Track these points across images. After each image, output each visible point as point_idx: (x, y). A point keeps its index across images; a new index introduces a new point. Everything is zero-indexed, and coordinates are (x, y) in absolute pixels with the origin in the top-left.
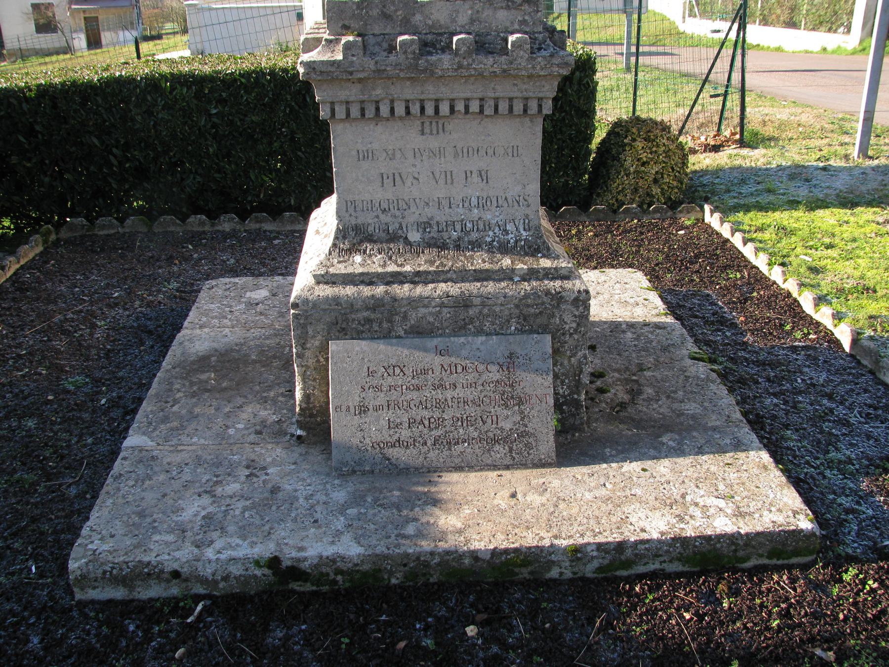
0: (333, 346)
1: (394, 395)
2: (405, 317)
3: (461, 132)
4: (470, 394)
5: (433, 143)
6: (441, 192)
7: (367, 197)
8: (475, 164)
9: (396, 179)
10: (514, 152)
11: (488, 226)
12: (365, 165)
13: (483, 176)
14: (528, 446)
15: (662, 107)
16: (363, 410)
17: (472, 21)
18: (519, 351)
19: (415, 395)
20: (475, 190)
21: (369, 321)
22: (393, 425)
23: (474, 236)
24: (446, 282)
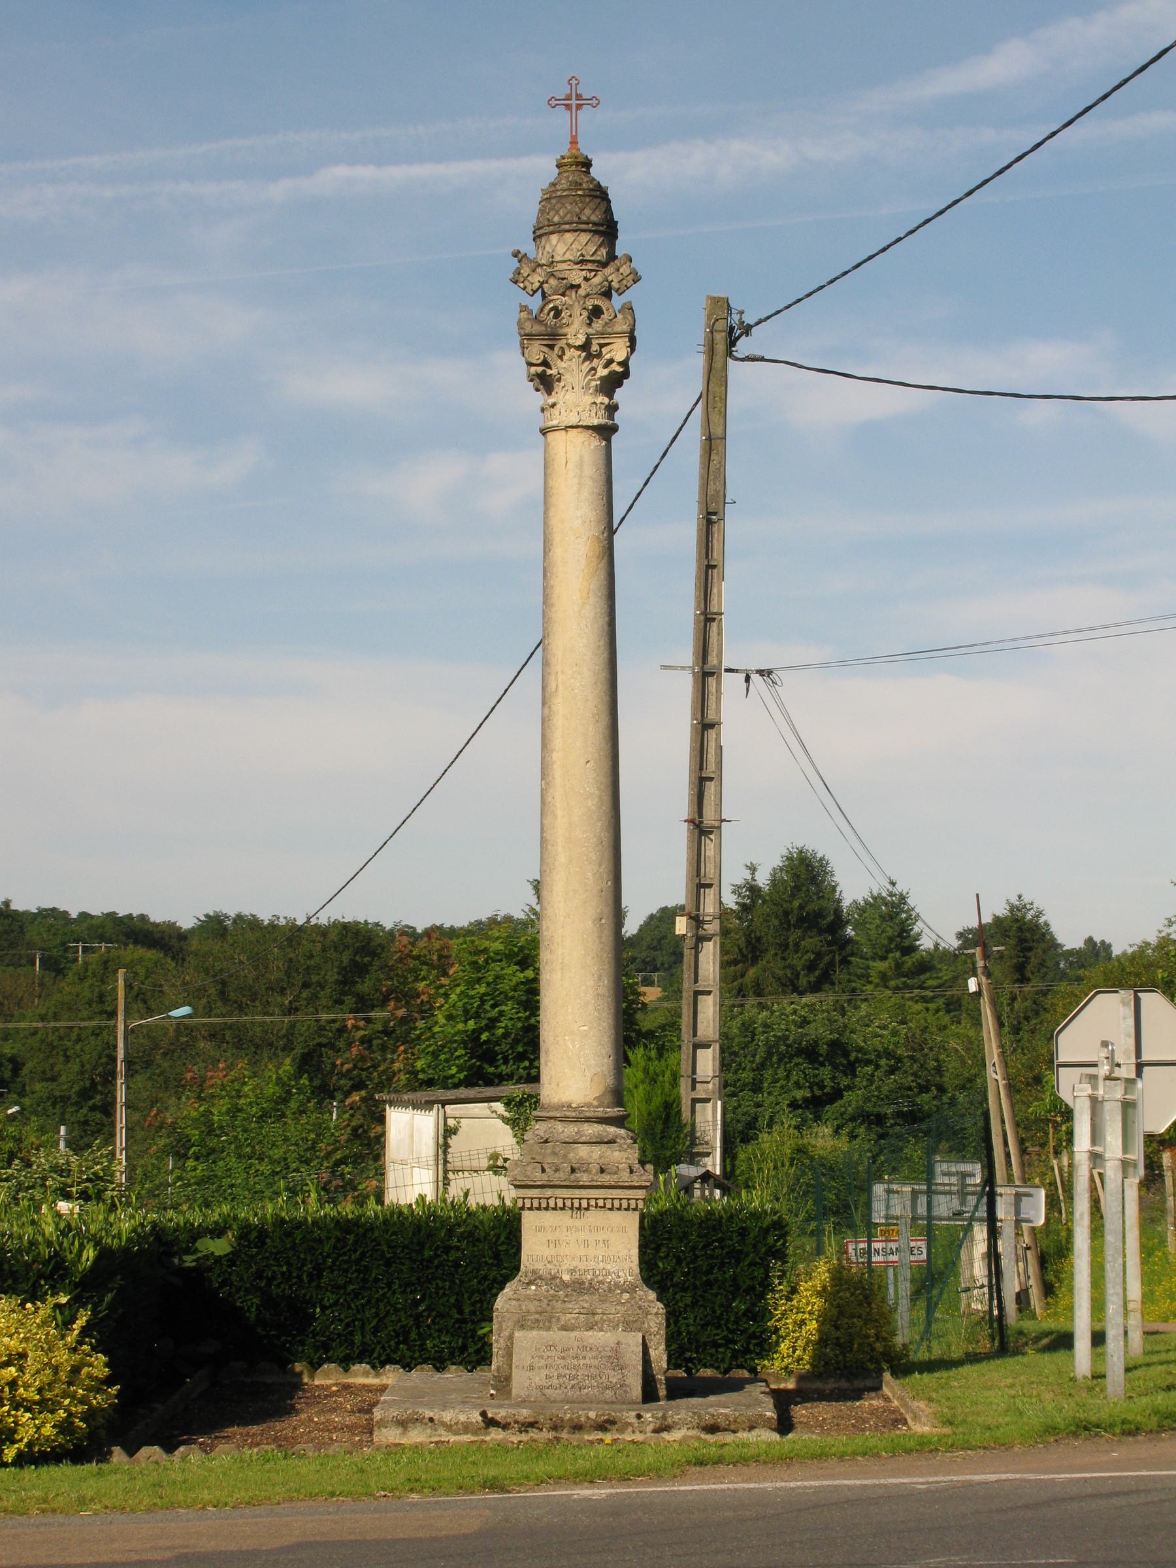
0: (517, 1334)
1: (550, 1361)
2: (559, 1319)
3: (594, 1217)
6: (582, 1252)
8: (601, 1236)
9: (556, 1243)
10: (624, 1230)
12: (540, 1235)
16: (532, 1368)
17: (601, 1157)
18: (623, 1341)
19: (561, 1361)
20: (601, 1251)
22: (548, 1377)
23: (601, 1278)
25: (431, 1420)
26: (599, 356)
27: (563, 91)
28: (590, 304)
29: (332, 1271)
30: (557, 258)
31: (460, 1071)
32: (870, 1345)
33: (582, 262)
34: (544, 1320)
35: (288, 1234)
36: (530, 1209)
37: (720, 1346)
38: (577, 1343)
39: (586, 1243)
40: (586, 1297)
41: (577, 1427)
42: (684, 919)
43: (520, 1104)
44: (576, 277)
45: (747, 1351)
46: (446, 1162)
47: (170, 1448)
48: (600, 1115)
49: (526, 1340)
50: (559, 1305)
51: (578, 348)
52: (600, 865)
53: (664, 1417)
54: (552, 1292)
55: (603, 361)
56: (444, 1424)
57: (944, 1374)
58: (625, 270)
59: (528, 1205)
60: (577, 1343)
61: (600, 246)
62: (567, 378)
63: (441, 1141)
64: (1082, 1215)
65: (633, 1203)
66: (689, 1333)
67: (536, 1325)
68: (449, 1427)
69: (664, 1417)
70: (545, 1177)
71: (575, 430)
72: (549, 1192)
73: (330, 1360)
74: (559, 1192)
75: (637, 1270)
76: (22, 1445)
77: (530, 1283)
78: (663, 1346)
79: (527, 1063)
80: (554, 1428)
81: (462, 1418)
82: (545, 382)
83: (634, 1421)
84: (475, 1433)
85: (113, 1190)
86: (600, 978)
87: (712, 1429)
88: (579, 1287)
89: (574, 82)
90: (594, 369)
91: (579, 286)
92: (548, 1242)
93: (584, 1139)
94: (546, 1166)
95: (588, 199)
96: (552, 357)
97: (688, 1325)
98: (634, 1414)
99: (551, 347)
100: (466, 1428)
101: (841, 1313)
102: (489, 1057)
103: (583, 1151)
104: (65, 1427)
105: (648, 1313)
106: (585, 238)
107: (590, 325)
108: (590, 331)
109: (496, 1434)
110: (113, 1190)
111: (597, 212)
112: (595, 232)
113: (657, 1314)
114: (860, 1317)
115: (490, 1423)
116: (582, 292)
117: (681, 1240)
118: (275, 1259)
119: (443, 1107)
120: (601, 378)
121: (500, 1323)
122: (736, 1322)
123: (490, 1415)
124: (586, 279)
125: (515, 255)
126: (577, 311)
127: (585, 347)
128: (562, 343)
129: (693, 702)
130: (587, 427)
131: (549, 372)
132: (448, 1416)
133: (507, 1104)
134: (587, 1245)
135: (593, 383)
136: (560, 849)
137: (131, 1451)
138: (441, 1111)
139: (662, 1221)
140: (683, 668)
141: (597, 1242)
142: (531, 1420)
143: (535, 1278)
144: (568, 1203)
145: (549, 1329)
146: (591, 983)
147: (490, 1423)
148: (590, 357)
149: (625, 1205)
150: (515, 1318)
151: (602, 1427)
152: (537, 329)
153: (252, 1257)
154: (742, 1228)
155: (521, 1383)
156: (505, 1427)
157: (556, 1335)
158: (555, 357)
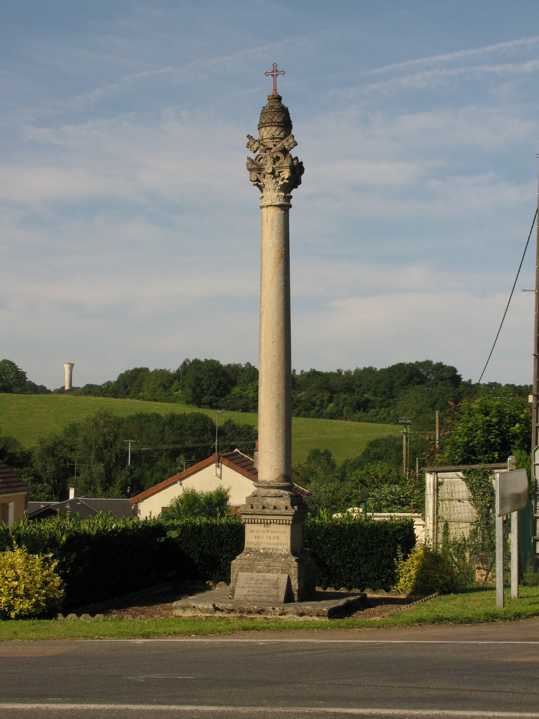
2: (256, 568)
3: (273, 527)
4: (268, 586)
5: (266, 529)
7: (252, 541)
8: (276, 535)
10: (285, 532)
11: (278, 550)
13: (278, 538)
14: (278, 598)
15: (51, 621)
16: (243, 587)
17: (276, 503)
18: (280, 577)
20: (276, 541)
21: (248, 568)
22: (249, 591)
24: (32, 550)
25: (194, 607)
26: (279, 176)
27: (279, 69)
28: (275, 156)
29: (226, 545)
30: (264, 137)
31: (459, 458)
32: (437, 581)
33: (273, 138)
34: (250, 568)
35: (210, 529)
36: (248, 523)
37: (377, 579)
38: (262, 578)
39: (270, 538)
40: (268, 559)
41: (250, 612)
42: (532, 396)
43: (469, 472)
44: (270, 145)
45: (387, 582)
46: (437, 496)
47: (93, 615)
48: (277, 485)
49: (243, 576)
50: (256, 562)
51: (270, 174)
52: (278, 384)
53: (283, 609)
54: (255, 557)
55: (281, 179)
56: (199, 609)
57: (484, 592)
58: (291, 141)
59: (247, 521)
60: (262, 578)
61: (281, 132)
62: (267, 186)
63: (435, 488)
64: (514, 529)
65: (288, 521)
66: (364, 574)
67: (247, 570)
68: (201, 610)
69: (283, 609)
70: (252, 510)
71: (271, 207)
72: (255, 517)
73: (222, 580)
74: (258, 517)
75: (289, 549)
76: (17, 612)
77: (247, 553)
78: (296, 580)
79: (488, 455)
80: (241, 612)
81: (206, 607)
82: (261, 188)
83: (272, 610)
84: (211, 613)
85: (414, 501)
86: (278, 430)
87: (301, 615)
88: (266, 555)
89: (275, 65)
90: (277, 182)
91: (271, 148)
92: (256, 536)
93: (269, 495)
94: (254, 506)
95: (276, 113)
96: (261, 177)
97: (364, 570)
98: (271, 607)
99: (260, 174)
100: (207, 611)
101: (425, 568)
102: (474, 453)
103: (269, 500)
104: (36, 605)
105: (291, 567)
106: (274, 128)
107: (274, 164)
108: (274, 166)
109: (218, 614)
110: (414, 501)
111: (280, 118)
112: (278, 126)
113: (294, 567)
114: (433, 569)
115: (216, 609)
116: (272, 151)
117: (361, 535)
118: (204, 539)
119: (437, 474)
120: (280, 185)
121: (233, 569)
122: (383, 569)
123: (216, 606)
124: (275, 145)
125: (248, 136)
126: (269, 158)
127: (273, 173)
128: (264, 172)
129: (536, 308)
130: (275, 206)
131: (260, 184)
132: (200, 606)
133: (464, 473)
134: (270, 539)
135: (277, 188)
136: (263, 377)
137: (65, 615)
138: (436, 475)
139: (354, 527)
140: (531, 291)
141: (274, 537)
142: (232, 608)
143: (250, 551)
144: (263, 521)
145: (252, 572)
146: (274, 432)
147: (216, 609)
148: (275, 177)
149: (284, 522)
150: (239, 567)
151: (260, 612)
152: (254, 166)
153: (196, 538)
154: (385, 531)
155: (239, 593)
156: (222, 611)
157: (255, 575)
158: (262, 178)
